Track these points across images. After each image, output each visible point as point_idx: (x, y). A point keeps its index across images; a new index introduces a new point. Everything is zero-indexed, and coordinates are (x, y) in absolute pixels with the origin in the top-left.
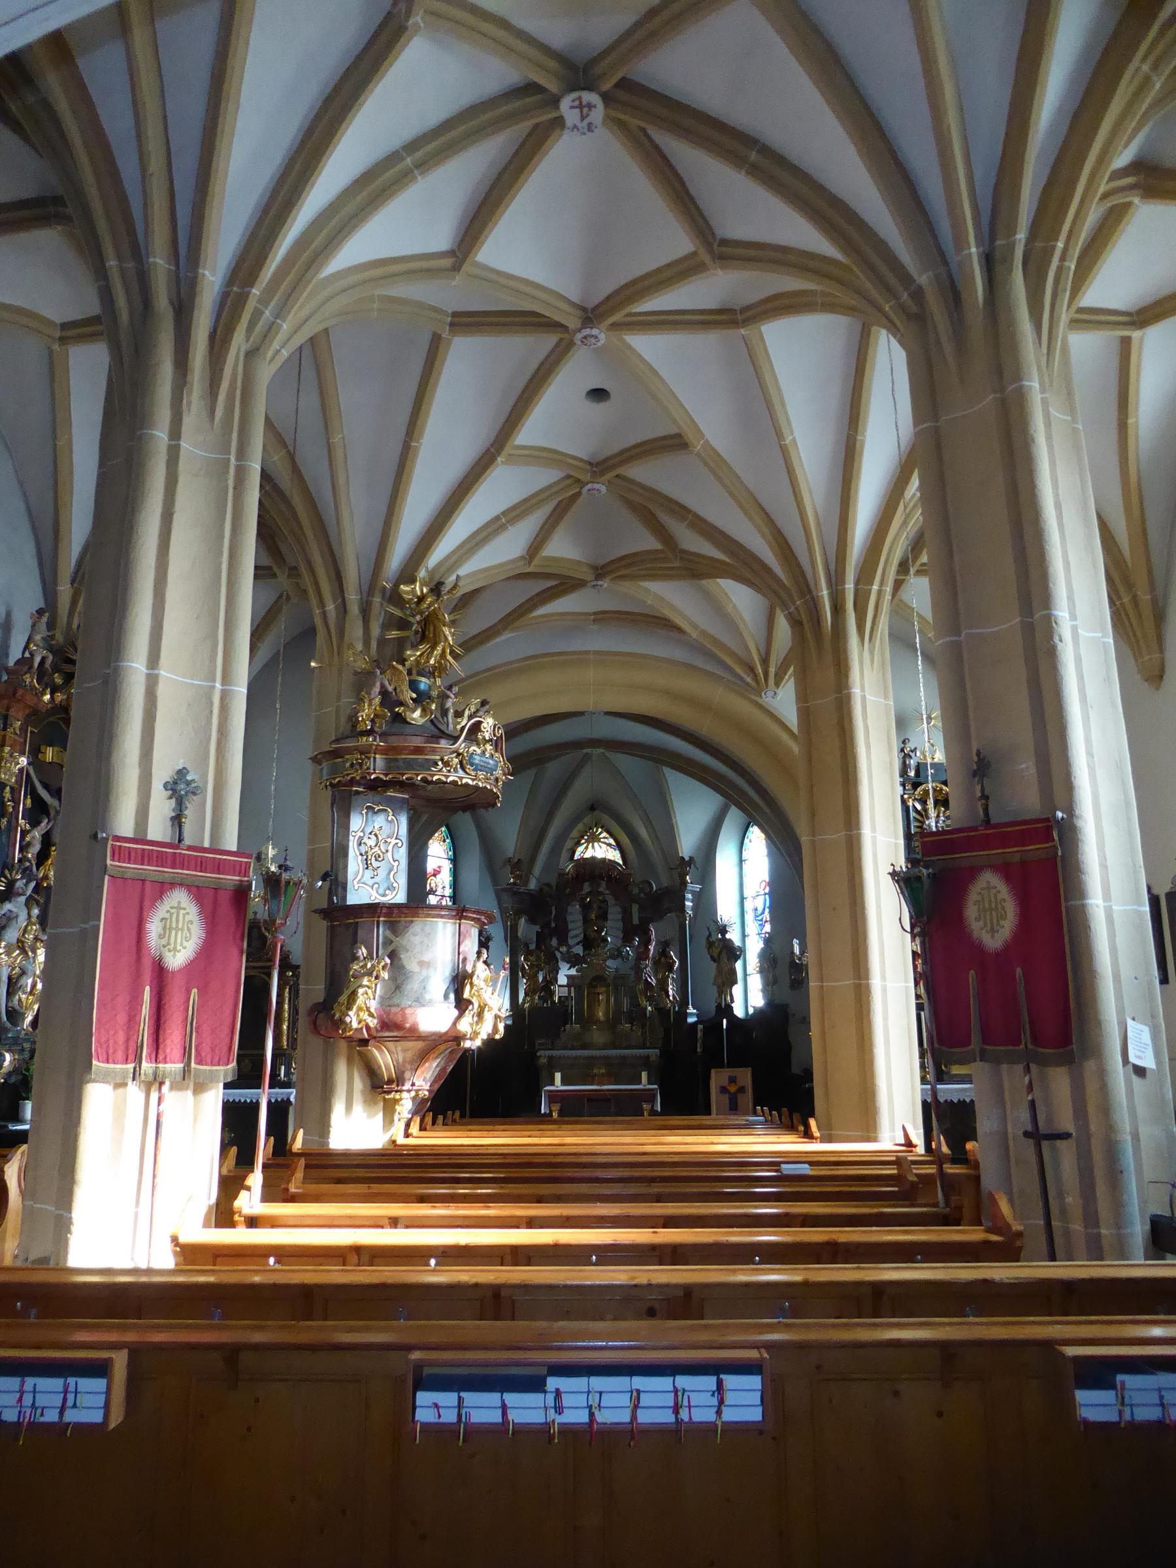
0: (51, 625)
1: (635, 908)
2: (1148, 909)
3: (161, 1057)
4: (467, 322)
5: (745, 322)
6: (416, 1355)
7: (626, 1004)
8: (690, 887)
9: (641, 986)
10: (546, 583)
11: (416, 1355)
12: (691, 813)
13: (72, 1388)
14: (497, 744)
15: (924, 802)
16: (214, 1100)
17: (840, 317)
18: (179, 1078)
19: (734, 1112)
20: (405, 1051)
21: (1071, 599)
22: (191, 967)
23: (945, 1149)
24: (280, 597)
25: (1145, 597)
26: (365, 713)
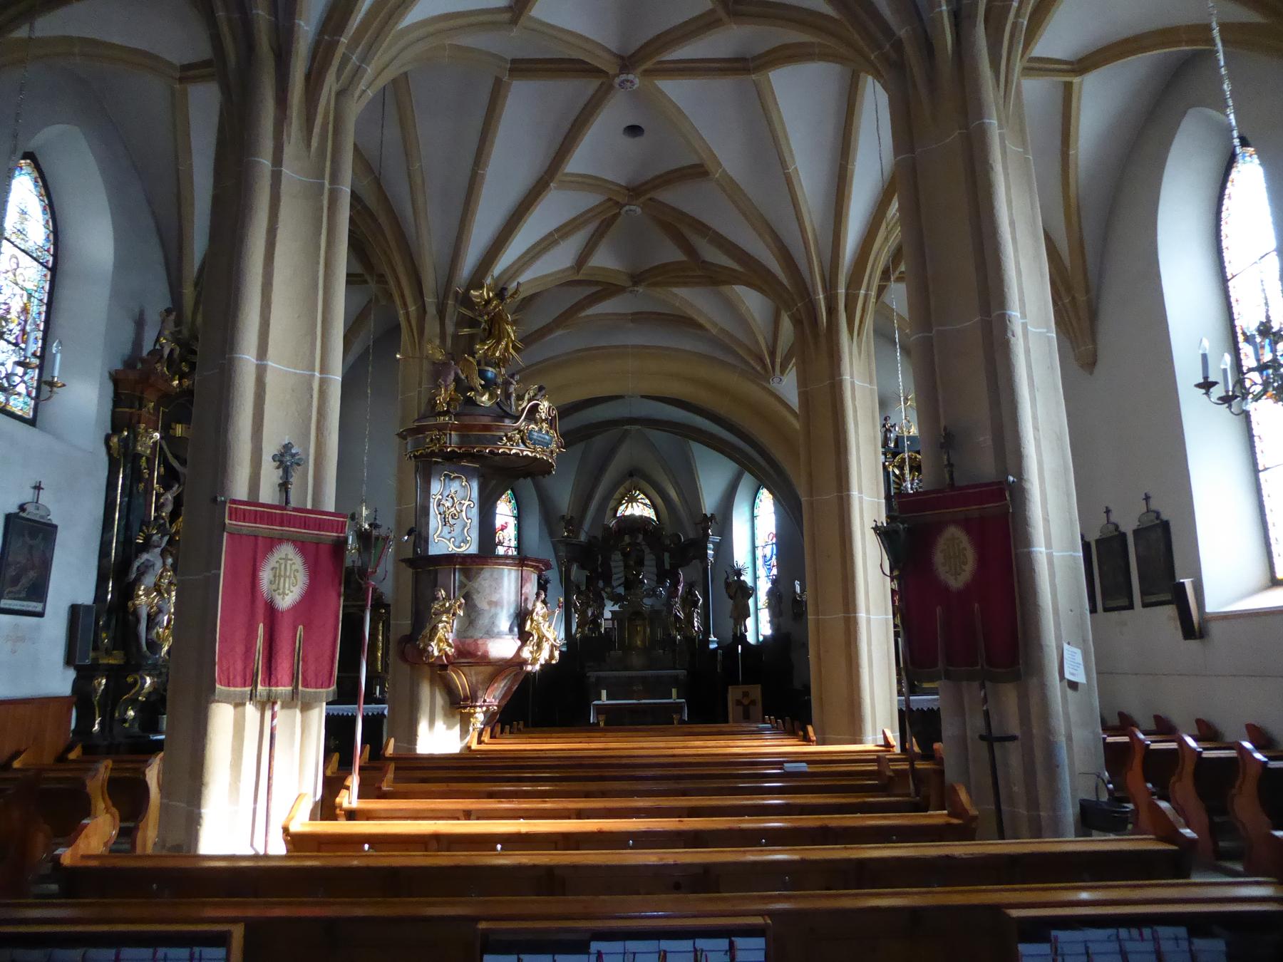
0: (178, 322)
1: (667, 555)
2: (1081, 554)
3: (273, 681)
4: (523, 68)
5: (757, 69)
6: (482, 925)
7: (659, 634)
8: (711, 538)
9: (672, 619)
10: (588, 287)
11: (482, 925)
12: (712, 480)
13: (197, 955)
14: (551, 423)
15: (901, 468)
16: (318, 717)
17: (833, 65)
18: (289, 699)
19: (747, 721)
20: (476, 674)
21: (1022, 301)
22: (296, 607)
23: (916, 749)
24: (370, 302)
25: (1081, 298)
26: (442, 397)
